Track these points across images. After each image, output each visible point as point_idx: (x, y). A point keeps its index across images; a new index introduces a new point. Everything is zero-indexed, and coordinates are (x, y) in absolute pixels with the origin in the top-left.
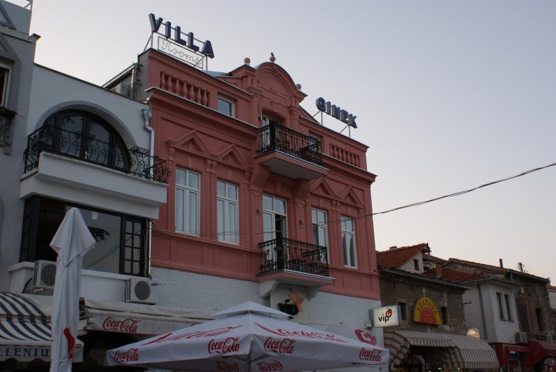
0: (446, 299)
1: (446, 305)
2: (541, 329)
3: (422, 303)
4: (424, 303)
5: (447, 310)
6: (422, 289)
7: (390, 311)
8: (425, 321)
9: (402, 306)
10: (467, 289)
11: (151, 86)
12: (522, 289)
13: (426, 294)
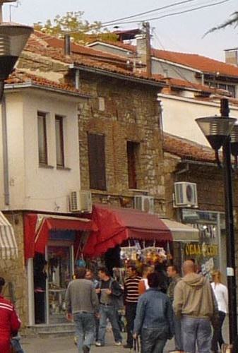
2: (133, 184)
11: (199, 69)
12: (102, 101)
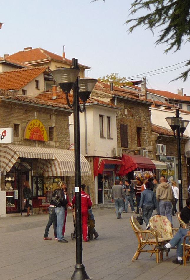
0: (54, 121)
1: (54, 125)
2: (139, 145)
3: (33, 124)
4: (34, 124)
5: (54, 128)
6: (34, 113)
7: (5, 132)
8: (34, 138)
9: (16, 127)
10: (36, 98)
12: (126, 110)
13: (37, 116)
